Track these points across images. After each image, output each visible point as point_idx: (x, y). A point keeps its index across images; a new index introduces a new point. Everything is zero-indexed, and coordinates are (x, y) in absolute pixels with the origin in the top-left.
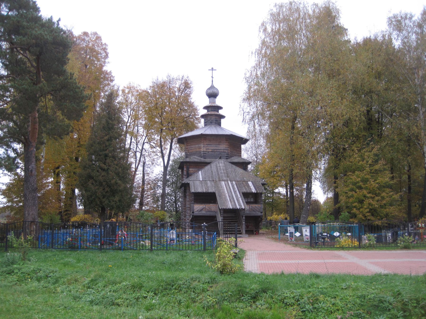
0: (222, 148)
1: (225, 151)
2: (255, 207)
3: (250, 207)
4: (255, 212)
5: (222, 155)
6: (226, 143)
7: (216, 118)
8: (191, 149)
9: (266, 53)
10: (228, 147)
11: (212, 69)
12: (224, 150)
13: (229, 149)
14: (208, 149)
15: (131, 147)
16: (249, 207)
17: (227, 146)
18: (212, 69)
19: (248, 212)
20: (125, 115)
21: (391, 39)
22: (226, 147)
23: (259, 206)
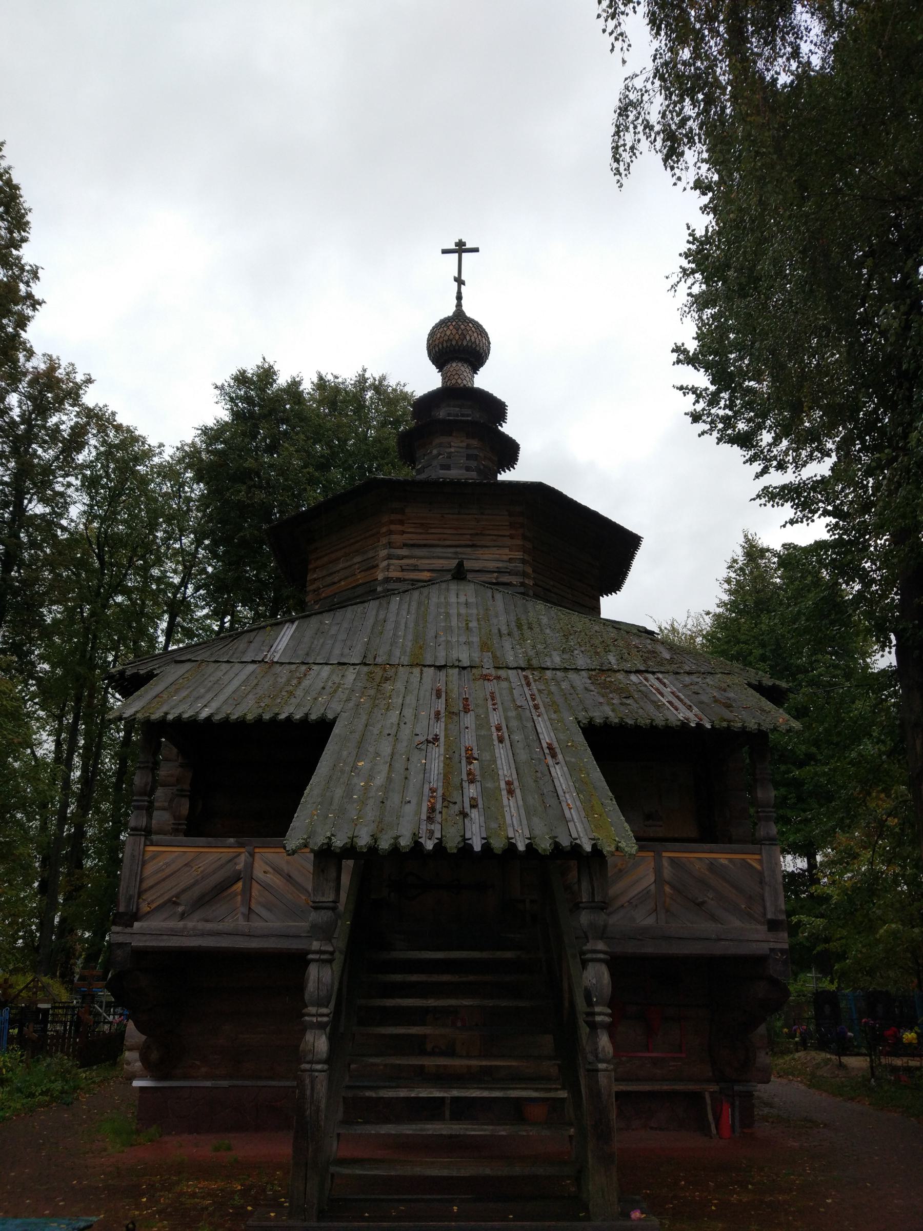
0: (492, 565)
1: (505, 579)
2: (712, 867)
3: (667, 872)
4: (713, 918)
5: (464, 556)
6: (511, 537)
7: (468, 447)
8: (329, 580)
9: (728, 79)
10: (523, 561)
11: (461, 248)
12: (499, 571)
13: (529, 570)
14: (416, 569)
15: (336, 662)
16: (658, 871)
17: (519, 555)
18: (461, 248)
19: (650, 921)
20: (69, 496)
21: (784, 487)
22: (510, 560)
23: (746, 865)
